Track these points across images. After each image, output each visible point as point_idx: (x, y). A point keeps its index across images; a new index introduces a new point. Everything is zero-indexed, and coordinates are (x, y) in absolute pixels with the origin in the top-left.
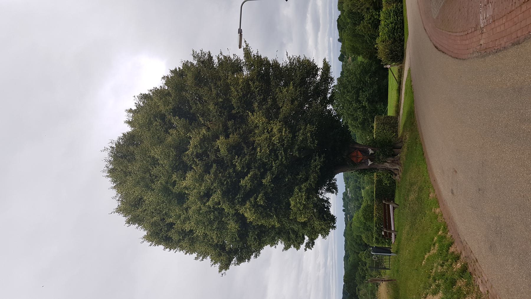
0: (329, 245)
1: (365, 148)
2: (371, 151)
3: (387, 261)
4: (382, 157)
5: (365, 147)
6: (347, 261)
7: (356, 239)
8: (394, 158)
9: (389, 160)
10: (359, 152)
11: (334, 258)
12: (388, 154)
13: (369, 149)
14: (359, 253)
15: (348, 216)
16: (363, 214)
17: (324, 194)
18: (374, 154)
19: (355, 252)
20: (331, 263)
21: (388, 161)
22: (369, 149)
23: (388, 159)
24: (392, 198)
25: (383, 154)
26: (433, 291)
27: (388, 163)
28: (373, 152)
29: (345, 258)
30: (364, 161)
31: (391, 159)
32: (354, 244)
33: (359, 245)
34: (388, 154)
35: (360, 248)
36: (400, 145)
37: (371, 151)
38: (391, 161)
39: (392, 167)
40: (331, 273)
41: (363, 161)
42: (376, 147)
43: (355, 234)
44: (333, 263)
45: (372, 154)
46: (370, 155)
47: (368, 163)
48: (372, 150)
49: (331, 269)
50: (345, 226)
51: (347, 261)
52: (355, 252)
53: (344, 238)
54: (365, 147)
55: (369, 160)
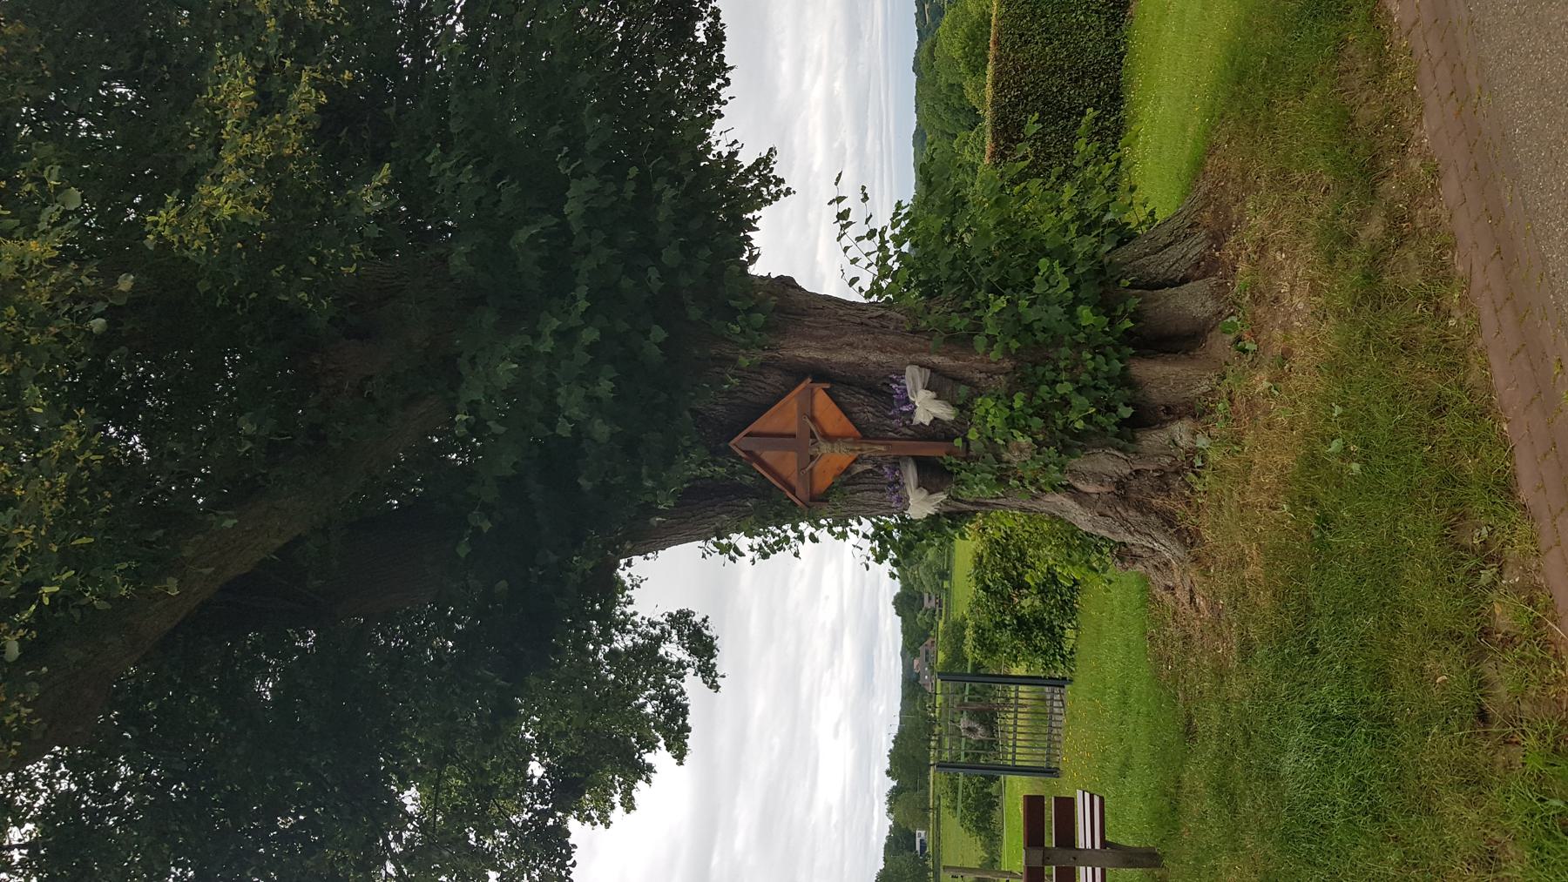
0: (871, 94)
1: (880, 364)
2: (927, 408)
3: (1024, 743)
5: (874, 357)
6: (922, 144)
7: (948, 97)
8: (1134, 440)
9: (1084, 476)
11: (884, 133)
14: (956, 137)
15: (927, 7)
16: (964, 52)
19: (943, 132)
20: (878, 148)
23: (1079, 463)
28: (945, 412)
29: (915, 136)
31: (1110, 464)
32: (940, 109)
33: (956, 111)
35: (958, 120)
36: (1193, 302)
37: (927, 408)
40: (877, 173)
43: (942, 81)
44: (881, 144)
49: (878, 165)
50: (917, 39)
51: (922, 144)
52: (943, 132)
53: (914, 77)
54: (874, 357)
55: (911, 475)
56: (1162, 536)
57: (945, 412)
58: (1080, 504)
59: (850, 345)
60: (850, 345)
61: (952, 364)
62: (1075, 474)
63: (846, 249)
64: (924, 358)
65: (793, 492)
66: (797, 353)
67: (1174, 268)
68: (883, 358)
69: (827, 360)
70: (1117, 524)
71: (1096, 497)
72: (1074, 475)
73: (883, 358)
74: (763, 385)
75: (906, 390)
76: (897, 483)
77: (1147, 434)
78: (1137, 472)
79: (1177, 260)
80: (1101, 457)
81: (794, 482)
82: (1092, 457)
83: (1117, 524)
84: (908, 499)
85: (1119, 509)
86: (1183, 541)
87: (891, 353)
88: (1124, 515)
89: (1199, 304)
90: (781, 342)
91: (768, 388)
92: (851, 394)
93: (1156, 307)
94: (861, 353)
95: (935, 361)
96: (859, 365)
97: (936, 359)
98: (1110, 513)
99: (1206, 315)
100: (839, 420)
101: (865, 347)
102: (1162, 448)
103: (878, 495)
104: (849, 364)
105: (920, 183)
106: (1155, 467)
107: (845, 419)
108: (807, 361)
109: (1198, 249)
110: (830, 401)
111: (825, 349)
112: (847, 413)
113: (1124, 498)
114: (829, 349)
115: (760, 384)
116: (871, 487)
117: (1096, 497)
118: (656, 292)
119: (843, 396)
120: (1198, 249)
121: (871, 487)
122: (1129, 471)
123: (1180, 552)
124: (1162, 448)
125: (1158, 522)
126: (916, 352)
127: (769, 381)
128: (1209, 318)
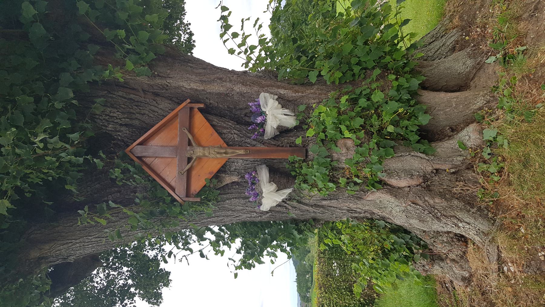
1: (241, 94)
4: (352, 154)
10: (199, 118)
12: (391, 129)
13: (263, 97)
17: (499, 143)
18: (300, 128)
21: (394, 182)
22: (263, 97)
23: (394, 164)
24: (164, 250)
25: (362, 134)
26: (107, 127)
27: (394, 191)
30: (235, 179)
34: (391, 129)
38: (414, 182)
39: (422, 221)
41: (228, 179)
42: (311, 84)
45: (283, 131)
46: (275, 138)
47: (258, 195)
48: (284, 102)
55: (264, 174)
56: (466, 215)
57: (290, 122)
58: (396, 196)
59: (221, 79)
60: (221, 79)
61: (294, 95)
62: (390, 173)
63: (225, 42)
64: (275, 90)
65: (173, 189)
66: (181, 84)
67: (438, 52)
68: (244, 89)
69: (203, 90)
70: (426, 212)
71: (407, 189)
72: (389, 174)
73: (244, 89)
74: (156, 109)
75: (259, 105)
76: (255, 182)
77: (440, 144)
78: (437, 170)
79: (440, 47)
80: (409, 158)
81: (173, 184)
82: (402, 158)
83: (426, 212)
84: (262, 193)
85: (426, 198)
86: (486, 217)
87: (250, 86)
88: (431, 202)
89: (461, 64)
90: (169, 71)
91: (160, 111)
92: (222, 121)
93: (431, 70)
94: (228, 85)
95: (282, 93)
96: (227, 95)
97: (282, 91)
98: (420, 202)
99: (468, 70)
100: (212, 135)
101: (231, 81)
102: (453, 152)
103: (242, 201)
104: (219, 94)
105: (285, 129)
106: (450, 166)
107: (216, 134)
108: (189, 91)
109: (453, 39)
110: (206, 121)
111: (202, 82)
112: (220, 134)
113: (428, 189)
114: (205, 82)
115: (153, 108)
116: (237, 195)
117: (407, 189)
118: (136, 149)
119: (216, 121)
120: (453, 39)
121: (237, 195)
122: (431, 168)
123: (484, 226)
124: (453, 152)
125: (461, 205)
126: (268, 86)
127: (160, 107)
128: (470, 72)
